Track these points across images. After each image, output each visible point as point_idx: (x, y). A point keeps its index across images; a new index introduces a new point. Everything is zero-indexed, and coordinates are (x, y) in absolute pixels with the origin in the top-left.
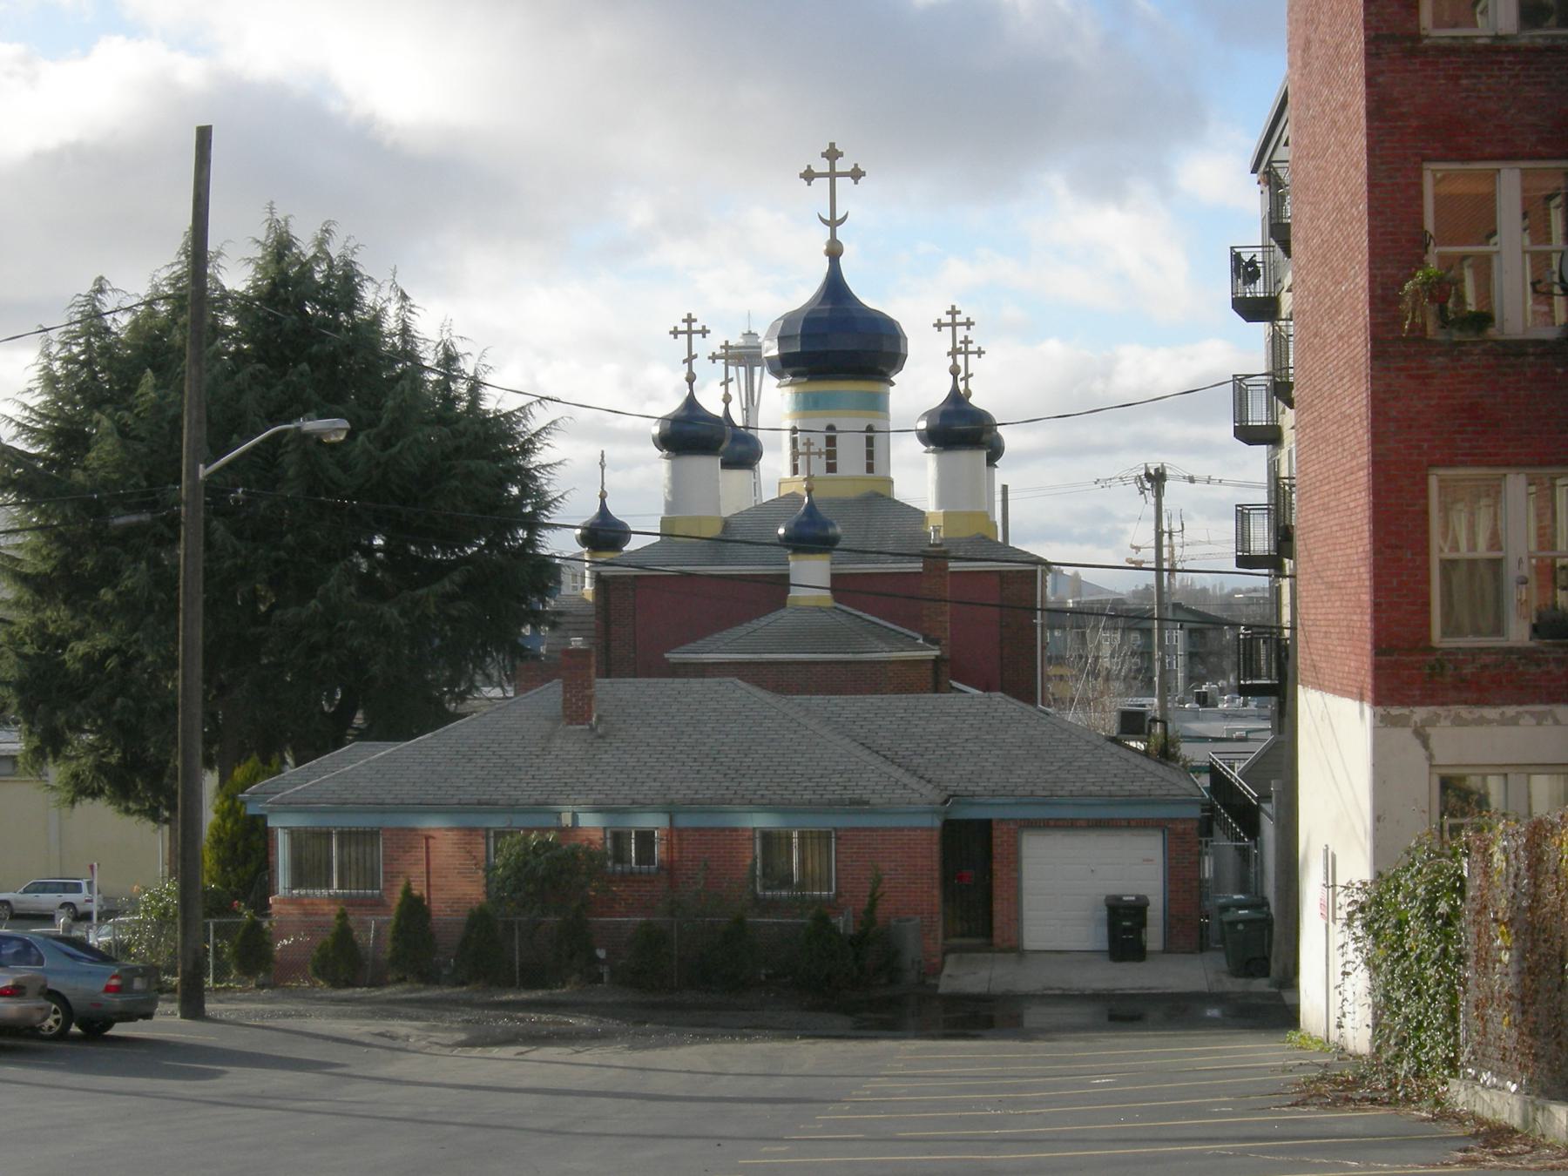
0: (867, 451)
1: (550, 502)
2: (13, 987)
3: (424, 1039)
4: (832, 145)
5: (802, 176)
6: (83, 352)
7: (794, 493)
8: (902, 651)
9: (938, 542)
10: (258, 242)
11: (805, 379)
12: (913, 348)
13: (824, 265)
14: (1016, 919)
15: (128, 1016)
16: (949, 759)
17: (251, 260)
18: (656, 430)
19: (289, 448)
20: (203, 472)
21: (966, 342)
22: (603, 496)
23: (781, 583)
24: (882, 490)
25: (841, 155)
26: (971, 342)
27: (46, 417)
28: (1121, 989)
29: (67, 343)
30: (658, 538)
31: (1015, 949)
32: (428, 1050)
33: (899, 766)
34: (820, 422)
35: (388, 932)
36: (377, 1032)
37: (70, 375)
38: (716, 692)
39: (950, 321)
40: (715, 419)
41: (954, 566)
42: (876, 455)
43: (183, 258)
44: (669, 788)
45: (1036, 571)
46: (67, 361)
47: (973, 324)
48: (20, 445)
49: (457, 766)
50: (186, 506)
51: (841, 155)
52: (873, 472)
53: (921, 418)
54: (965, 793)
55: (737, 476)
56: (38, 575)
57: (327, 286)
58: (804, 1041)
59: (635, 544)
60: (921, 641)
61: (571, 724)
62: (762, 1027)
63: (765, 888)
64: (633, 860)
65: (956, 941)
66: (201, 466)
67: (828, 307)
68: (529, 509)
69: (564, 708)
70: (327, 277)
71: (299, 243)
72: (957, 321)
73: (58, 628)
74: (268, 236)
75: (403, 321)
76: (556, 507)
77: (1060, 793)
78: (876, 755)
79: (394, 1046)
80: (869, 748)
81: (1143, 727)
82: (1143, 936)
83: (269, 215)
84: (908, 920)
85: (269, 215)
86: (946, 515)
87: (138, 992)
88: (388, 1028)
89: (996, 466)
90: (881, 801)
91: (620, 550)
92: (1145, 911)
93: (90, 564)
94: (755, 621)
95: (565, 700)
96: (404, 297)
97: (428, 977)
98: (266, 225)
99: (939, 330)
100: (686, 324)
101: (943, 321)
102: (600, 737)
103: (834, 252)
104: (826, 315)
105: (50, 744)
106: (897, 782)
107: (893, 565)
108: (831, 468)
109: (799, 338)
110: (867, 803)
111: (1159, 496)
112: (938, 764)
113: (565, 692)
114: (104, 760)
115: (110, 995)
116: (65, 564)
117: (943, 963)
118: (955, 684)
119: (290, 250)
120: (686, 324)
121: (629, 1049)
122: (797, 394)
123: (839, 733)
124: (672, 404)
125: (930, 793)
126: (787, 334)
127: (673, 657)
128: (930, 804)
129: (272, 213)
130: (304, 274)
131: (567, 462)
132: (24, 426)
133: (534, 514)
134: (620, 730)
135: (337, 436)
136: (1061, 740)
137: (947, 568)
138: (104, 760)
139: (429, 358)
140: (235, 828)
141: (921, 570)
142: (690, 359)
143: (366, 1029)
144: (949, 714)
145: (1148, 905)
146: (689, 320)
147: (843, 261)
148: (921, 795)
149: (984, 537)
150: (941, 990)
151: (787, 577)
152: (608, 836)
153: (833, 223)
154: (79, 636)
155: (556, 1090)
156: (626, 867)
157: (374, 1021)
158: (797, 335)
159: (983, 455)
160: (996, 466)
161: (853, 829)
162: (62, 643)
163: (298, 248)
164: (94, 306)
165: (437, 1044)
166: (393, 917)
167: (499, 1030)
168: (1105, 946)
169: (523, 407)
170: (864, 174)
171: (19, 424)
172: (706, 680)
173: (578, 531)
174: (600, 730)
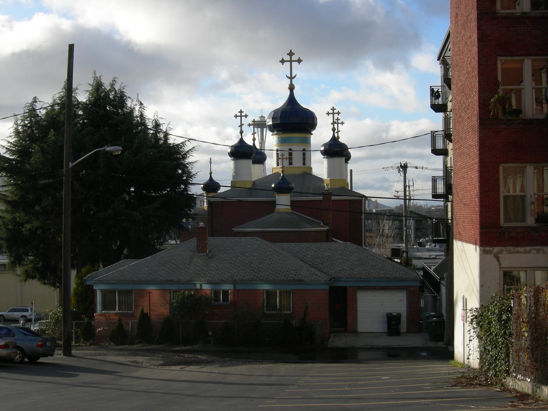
4: (291, 51)
5: (280, 61)
8: (315, 227)
9: (328, 189)
10: (90, 84)
11: (281, 133)
12: (319, 122)
15: (45, 355)
18: (229, 150)
20: (71, 165)
22: (211, 173)
23: (273, 204)
25: (294, 54)
29: (23, 120)
30: (230, 188)
31: (355, 332)
32: (149, 367)
33: (314, 268)
34: (286, 148)
37: (24, 131)
38: (250, 242)
39: (240, 115)
41: (333, 198)
43: (64, 90)
44: (234, 275)
45: (362, 200)
47: (340, 113)
48: (7, 156)
51: (294, 54)
53: (322, 146)
54: (337, 277)
55: (257, 167)
57: (114, 100)
58: (281, 364)
59: (222, 190)
60: (322, 224)
63: (267, 310)
64: (221, 301)
66: (70, 163)
67: (289, 107)
68: (185, 178)
71: (104, 85)
73: (20, 220)
74: (94, 83)
75: (141, 112)
76: (194, 177)
77: (370, 277)
78: (306, 264)
79: (138, 366)
92: (400, 318)
93: (32, 197)
94: (264, 217)
95: (197, 245)
97: (150, 341)
98: (93, 79)
99: (328, 115)
102: (210, 257)
103: (292, 88)
105: (17, 260)
108: (291, 164)
109: (279, 118)
110: (303, 281)
111: (405, 173)
113: (197, 242)
114: (36, 266)
118: (334, 239)
120: (240, 113)
121: (220, 367)
122: (279, 138)
127: (235, 229)
128: (325, 281)
132: (8, 149)
133: (187, 180)
134: (217, 255)
137: (331, 198)
138: (36, 266)
139: (150, 125)
141: (322, 199)
143: (128, 360)
144: (332, 250)
145: (401, 316)
146: (241, 112)
147: (295, 91)
148: (322, 278)
149: (344, 188)
150: (329, 346)
151: (275, 202)
152: (213, 292)
153: (291, 78)
154: (28, 222)
158: (278, 117)
162: (22, 225)
163: (104, 87)
166: (137, 321)
168: (386, 331)
169: (183, 142)
170: (302, 61)
171: (6, 148)
174: (210, 255)
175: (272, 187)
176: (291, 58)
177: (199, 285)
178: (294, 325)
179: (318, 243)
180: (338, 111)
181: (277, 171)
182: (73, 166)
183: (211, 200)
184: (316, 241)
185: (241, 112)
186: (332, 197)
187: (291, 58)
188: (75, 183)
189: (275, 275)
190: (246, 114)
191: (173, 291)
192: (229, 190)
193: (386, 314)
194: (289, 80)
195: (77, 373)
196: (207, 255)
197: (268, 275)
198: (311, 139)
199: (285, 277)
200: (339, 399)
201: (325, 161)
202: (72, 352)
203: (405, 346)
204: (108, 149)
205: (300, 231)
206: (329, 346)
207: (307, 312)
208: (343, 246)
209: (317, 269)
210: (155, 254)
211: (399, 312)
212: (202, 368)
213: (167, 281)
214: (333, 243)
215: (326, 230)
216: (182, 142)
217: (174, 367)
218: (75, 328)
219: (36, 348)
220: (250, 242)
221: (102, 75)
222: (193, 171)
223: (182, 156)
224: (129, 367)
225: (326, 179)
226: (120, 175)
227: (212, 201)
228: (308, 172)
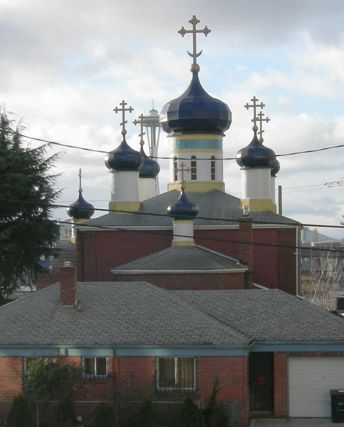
4: (194, 17)
5: (179, 32)
7: (175, 189)
8: (229, 268)
9: (247, 214)
11: (181, 133)
13: (190, 77)
14: (286, 401)
18: (107, 158)
23: (169, 234)
24: (218, 187)
25: (199, 21)
30: (108, 212)
33: (228, 325)
38: (137, 288)
40: (136, 153)
41: (254, 226)
45: (295, 229)
47: (245, 106)
51: (199, 21)
53: (238, 153)
54: (260, 339)
55: (147, 182)
59: (96, 215)
60: (238, 263)
61: (64, 305)
63: (161, 386)
64: (96, 372)
65: (255, 412)
68: (44, 198)
72: (125, 108)
76: (57, 197)
84: (232, 402)
86: (250, 200)
89: (276, 177)
91: (89, 218)
99: (248, 109)
102: (79, 311)
103: (195, 70)
106: (226, 333)
110: (212, 344)
112: (247, 325)
113: (61, 289)
117: (249, 423)
118: (255, 285)
122: (177, 140)
124: (115, 146)
126: (172, 110)
128: (243, 344)
131: (62, 174)
133: (46, 200)
134: (89, 307)
137: (252, 227)
141: (238, 228)
142: (124, 123)
146: (123, 104)
147: (201, 76)
148: (239, 340)
149: (270, 212)
152: (83, 360)
153: (195, 56)
156: (92, 375)
158: (177, 111)
159: (269, 171)
168: (330, 415)
169: (41, 147)
173: (68, 209)
174: (79, 308)
175: (168, 211)
176: (194, 27)
177: (64, 350)
181: (175, 189)
183: (80, 230)
186: (253, 225)
187: (194, 27)
190: (267, 118)
193: (329, 391)
196: (75, 307)
198: (223, 141)
199: (185, 339)
205: (208, 274)
215: (245, 272)
216: (39, 146)
222: (55, 188)
225: (244, 200)
227: (82, 231)
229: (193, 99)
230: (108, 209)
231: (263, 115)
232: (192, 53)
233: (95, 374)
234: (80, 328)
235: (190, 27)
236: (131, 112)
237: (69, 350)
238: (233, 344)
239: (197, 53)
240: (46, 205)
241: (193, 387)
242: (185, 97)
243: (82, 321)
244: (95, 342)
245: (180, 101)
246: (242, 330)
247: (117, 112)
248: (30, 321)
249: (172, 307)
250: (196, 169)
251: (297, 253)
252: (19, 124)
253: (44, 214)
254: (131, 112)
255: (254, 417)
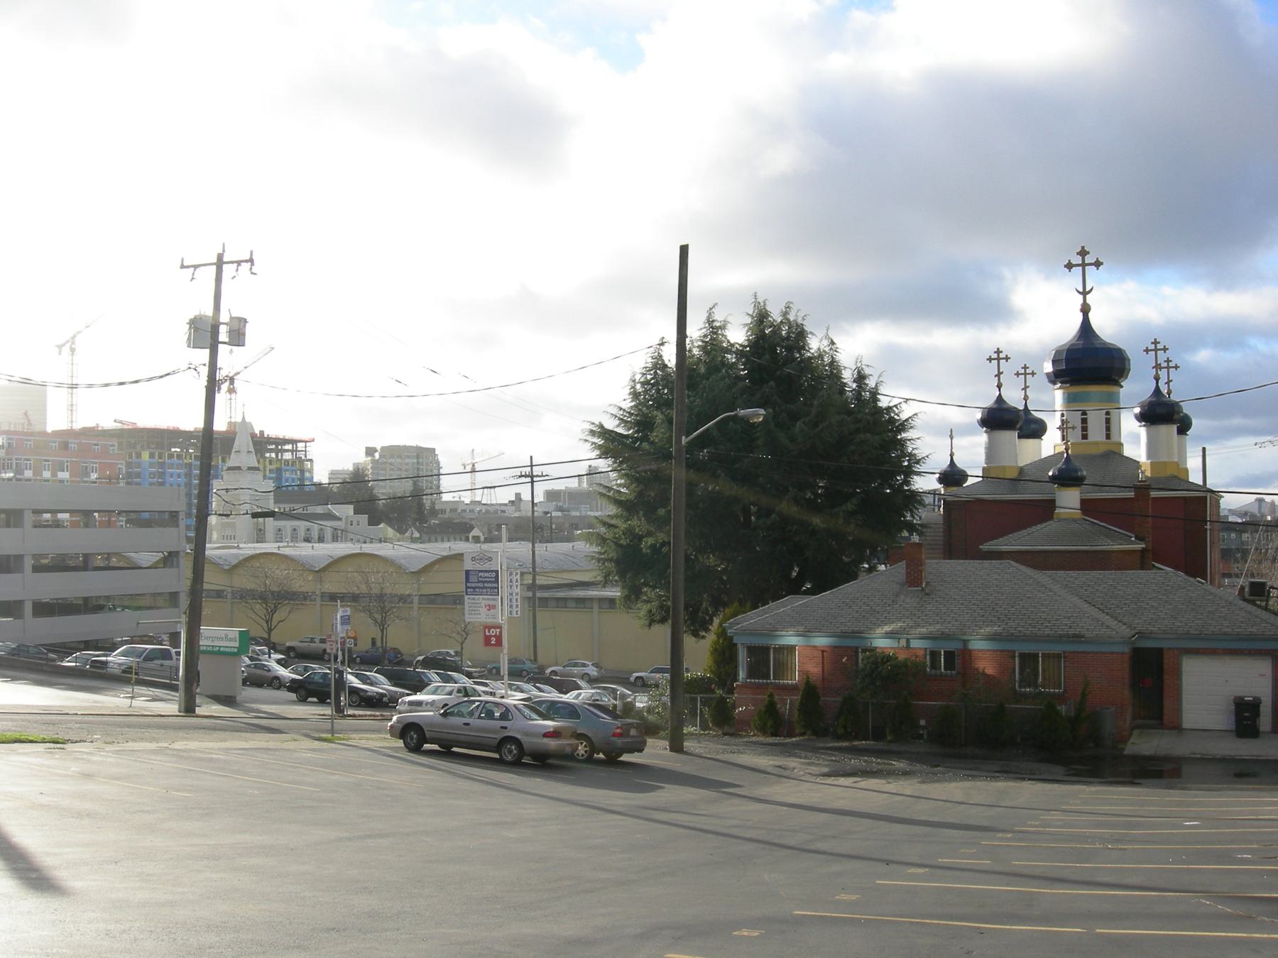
0: (1106, 427)
1: (920, 459)
2: (553, 732)
3: (803, 770)
4: (1083, 247)
5: (1065, 266)
6: (652, 379)
9: (1144, 479)
10: (749, 315)
11: (1068, 385)
12: (1134, 365)
13: (1080, 317)
14: (1178, 710)
15: (631, 751)
16: (1138, 611)
17: (746, 325)
18: (979, 416)
19: (759, 429)
20: (684, 440)
21: (1168, 361)
22: (952, 455)
25: (1088, 253)
26: (1171, 361)
27: (631, 414)
28: (1240, 756)
29: (644, 374)
30: (981, 479)
31: (1177, 728)
32: (803, 778)
33: (1107, 614)
35: (797, 704)
36: (778, 764)
37: (646, 392)
38: (998, 568)
39: (1154, 348)
40: (1015, 410)
41: (1154, 494)
42: (1089, 429)
43: (707, 325)
44: (965, 625)
45: (1206, 497)
46: (643, 384)
48: (620, 430)
49: (842, 610)
50: (675, 459)
51: (1088, 253)
52: (1087, 439)
54: (1147, 632)
55: (1030, 443)
56: (627, 500)
57: (788, 338)
58: (1029, 782)
59: (970, 481)
60: (1133, 539)
61: (910, 587)
62: (1007, 772)
63: (1020, 687)
64: (943, 668)
65: (1139, 722)
67: (1082, 342)
68: (906, 464)
69: (907, 577)
70: (788, 333)
71: (772, 315)
72: (1158, 348)
73: (640, 531)
74: (754, 312)
75: (832, 356)
76: (924, 463)
77: (1206, 632)
78: (1093, 607)
79: (782, 774)
80: (1090, 603)
81: (1264, 592)
82: (1258, 722)
83: (754, 300)
84: (1108, 709)
85: (754, 300)
87: (633, 737)
88: (785, 763)
89: (1187, 435)
90: (1092, 635)
91: (961, 485)
92: (1259, 706)
93: (653, 494)
94: (1034, 527)
95: (907, 573)
96: (833, 343)
97: (820, 733)
98: (753, 305)
100: (996, 354)
101: (1005, 360)
102: (927, 594)
103: (1085, 309)
104: (1081, 347)
105: (633, 595)
106: (1102, 624)
107: (1118, 494)
108: (1085, 437)
110: (1083, 637)
112: (1131, 614)
113: (907, 568)
114: (664, 603)
115: (616, 738)
116: (640, 495)
117: (1131, 735)
118: (1157, 565)
119: (767, 319)
120: (996, 354)
121: (920, 783)
122: (1064, 393)
123: (1072, 594)
124: (989, 402)
125: (1125, 631)
127: (985, 547)
128: (1122, 638)
129: (756, 299)
130: (775, 332)
132: (622, 419)
133: (909, 466)
134: (939, 590)
135: (757, 418)
136: (1209, 599)
137: (1150, 495)
138: (664, 603)
139: (848, 376)
140: (725, 643)
142: (999, 375)
143: (771, 763)
144: (1140, 583)
145: (1261, 703)
146: (1025, 368)
147: (1092, 317)
148: (1117, 632)
149: (1175, 477)
150: (1126, 752)
151: (1054, 501)
152: (928, 653)
153: (1085, 293)
154: (649, 534)
155: (836, 810)
156: (938, 671)
157: (780, 758)
159: (1174, 428)
160: (1187, 435)
161: (1074, 652)
162: (640, 538)
163: (772, 317)
164: (659, 353)
165: (810, 774)
166: (799, 697)
167: (849, 767)
168: (1233, 727)
170: (1102, 264)
171: (619, 419)
172: (993, 561)
173: (937, 476)
174: (927, 591)
175: (1050, 476)
176: (1083, 260)
177: (905, 640)
178: (1064, 714)
179: (985, 561)
180: (1165, 346)
182: (687, 443)
184: (1121, 567)
185: (1025, 368)
187: (1083, 260)
188: (719, 471)
189: (1035, 627)
190: (1033, 371)
191: (862, 649)
192: (978, 482)
193: (1233, 698)
194: (1081, 297)
195: (662, 785)
197: (1023, 627)
199: (1051, 630)
200: (1148, 842)
201: (1142, 432)
202: (685, 744)
203: (1265, 758)
204: (742, 412)
206: (1126, 752)
207: (1087, 692)
208: (1160, 576)
209: (1112, 617)
210: (836, 587)
211: (1258, 696)
212: (889, 783)
213: (852, 633)
214: (1155, 571)
217: (843, 779)
218: (700, 706)
219: (612, 739)
220: (998, 568)
221: (766, 300)
222: (920, 453)
223: (897, 427)
224: (766, 775)
225: (1145, 463)
226: (762, 456)
228: (1116, 451)
229: (1082, 344)
230: (981, 475)
231: (1028, 368)
232: (1081, 290)
233: (943, 670)
234: (926, 615)
235: (1078, 260)
236: (1007, 361)
237: (911, 640)
238: (1109, 637)
239: (1087, 290)
240: (909, 472)
241: (795, 680)
242: (1074, 342)
243: (929, 607)
244: (942, 632)
245: (1067, 347)
246: (1125, 620)
247: (990, 362)
248: (868, 605)
249: (1039, 591)
250: (1082, 423)
251: (1208, 527)
252: (878, 378)
253: (907, 482)
254: (1007, 361)
255: (1138, 727)
